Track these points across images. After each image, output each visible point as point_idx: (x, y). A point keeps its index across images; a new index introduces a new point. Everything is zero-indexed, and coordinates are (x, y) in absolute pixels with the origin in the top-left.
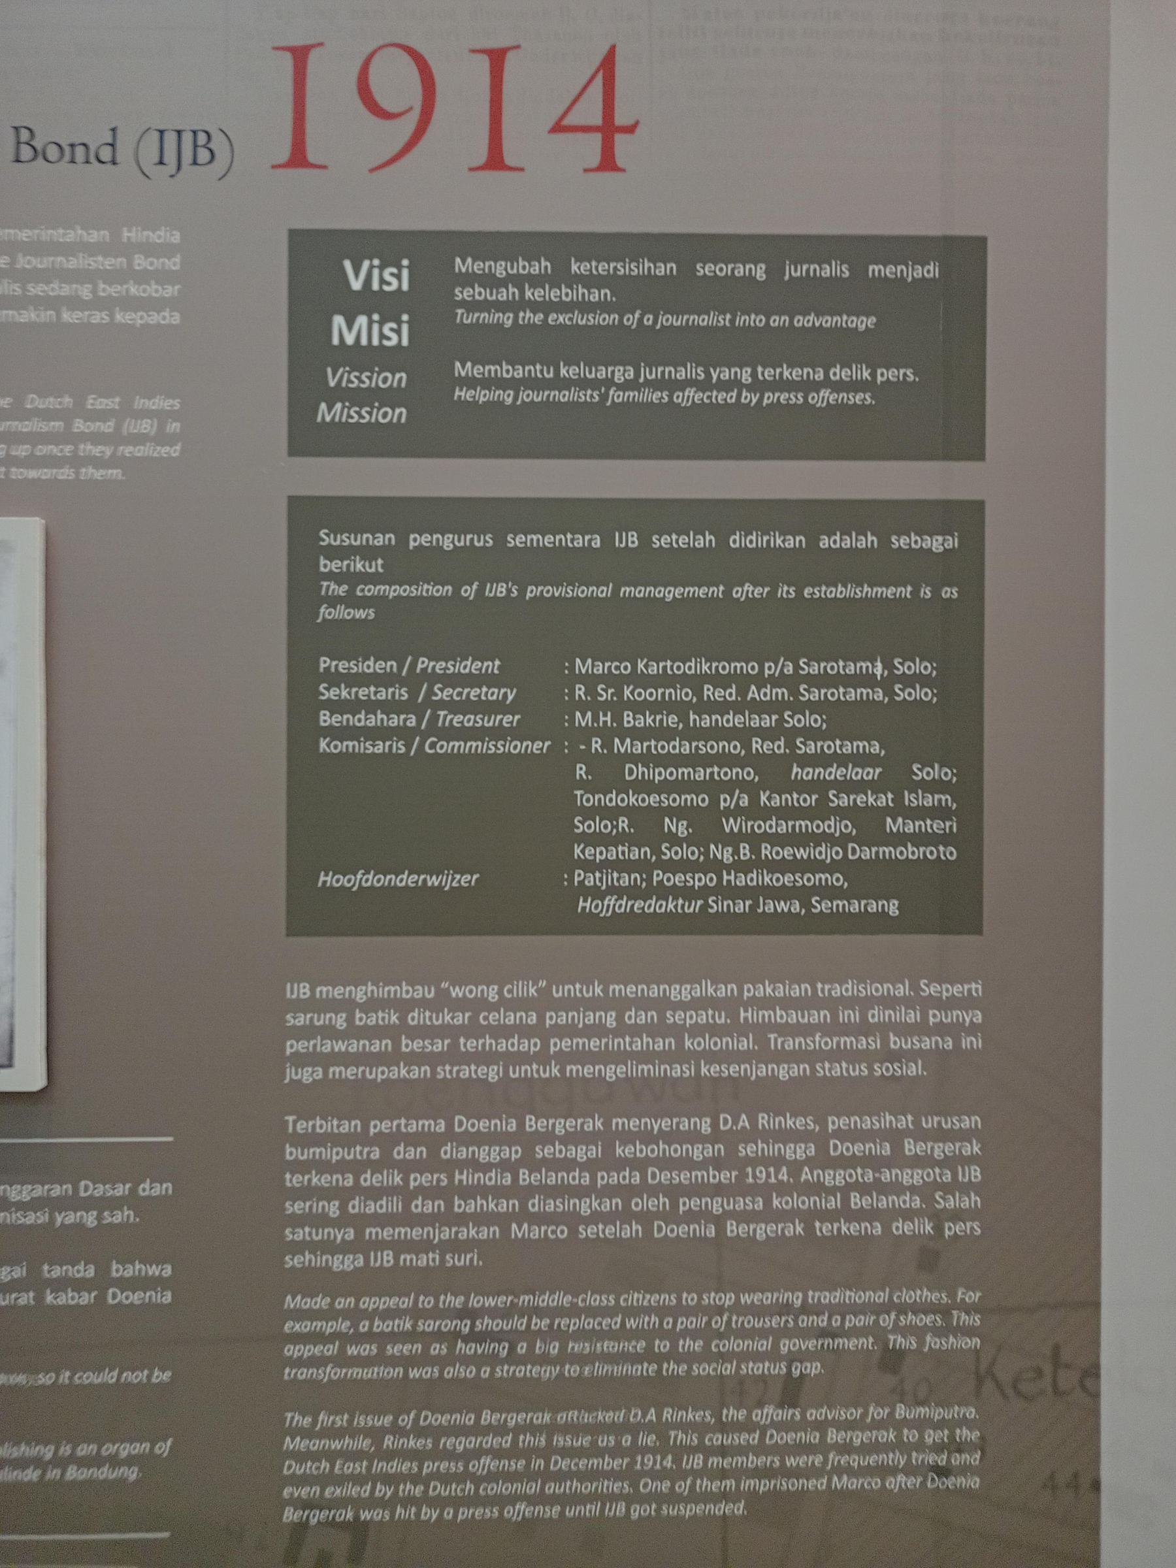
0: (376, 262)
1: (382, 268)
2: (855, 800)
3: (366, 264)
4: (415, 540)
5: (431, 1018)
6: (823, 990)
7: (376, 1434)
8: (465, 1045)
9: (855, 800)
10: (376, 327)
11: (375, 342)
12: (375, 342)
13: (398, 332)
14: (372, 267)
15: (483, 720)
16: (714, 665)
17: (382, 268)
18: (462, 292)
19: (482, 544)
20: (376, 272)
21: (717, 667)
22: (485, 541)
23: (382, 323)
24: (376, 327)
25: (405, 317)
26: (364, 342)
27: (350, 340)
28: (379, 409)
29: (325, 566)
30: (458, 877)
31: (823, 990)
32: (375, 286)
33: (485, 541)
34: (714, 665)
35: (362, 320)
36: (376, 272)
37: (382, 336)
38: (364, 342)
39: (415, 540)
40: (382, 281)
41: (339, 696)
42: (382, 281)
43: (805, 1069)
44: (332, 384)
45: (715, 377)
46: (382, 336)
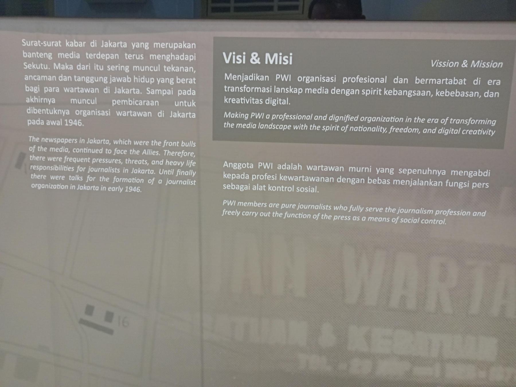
0: (234, 53)
1: (236, 55)
2: (231, 100)
3: (231, 54)
4: (475, 185)
5: (99, 68)
6: (227, 89)
7: (54, 50)
8: (166, 69)
9: (231, 100)
10: (281, 57)
11: (280, 63)
12: (280, 63)
13: (289, 59)
14: (232, 55)
15: (465, 122)
16: (229, 99)
17: (236, 55)
18: (402, 170)
19: (139, 58)
20: (234, 57)
21: (287, 189)
22: (140, 57)
23: (283, 56)
24: (281, 57)
25: (291, 54)
26: (276, 63)
27: (271, 62)
28: (449, 62)
29: (418, 81)
30: (385, 118)
31: (227, 89)
32: (234, 62)
33: (140, 57)
34: (229, 99)
35: (276, 55)
36: (234, 57)
37: (283, 61)
38: (276, 63)
39: (475, 185)
40: (236, 60)
41: (32, 67)
42: (236, 60)
43: (342, 169)
44: (433, 66)
45: (378, 172)
46: (283, 61)
